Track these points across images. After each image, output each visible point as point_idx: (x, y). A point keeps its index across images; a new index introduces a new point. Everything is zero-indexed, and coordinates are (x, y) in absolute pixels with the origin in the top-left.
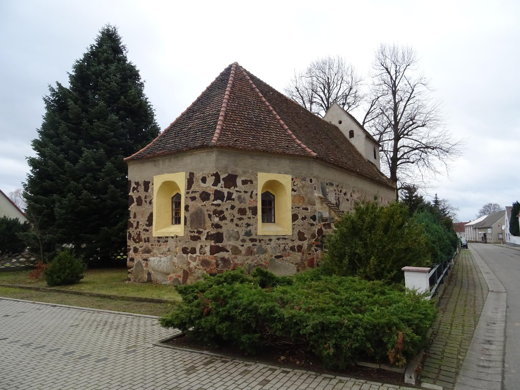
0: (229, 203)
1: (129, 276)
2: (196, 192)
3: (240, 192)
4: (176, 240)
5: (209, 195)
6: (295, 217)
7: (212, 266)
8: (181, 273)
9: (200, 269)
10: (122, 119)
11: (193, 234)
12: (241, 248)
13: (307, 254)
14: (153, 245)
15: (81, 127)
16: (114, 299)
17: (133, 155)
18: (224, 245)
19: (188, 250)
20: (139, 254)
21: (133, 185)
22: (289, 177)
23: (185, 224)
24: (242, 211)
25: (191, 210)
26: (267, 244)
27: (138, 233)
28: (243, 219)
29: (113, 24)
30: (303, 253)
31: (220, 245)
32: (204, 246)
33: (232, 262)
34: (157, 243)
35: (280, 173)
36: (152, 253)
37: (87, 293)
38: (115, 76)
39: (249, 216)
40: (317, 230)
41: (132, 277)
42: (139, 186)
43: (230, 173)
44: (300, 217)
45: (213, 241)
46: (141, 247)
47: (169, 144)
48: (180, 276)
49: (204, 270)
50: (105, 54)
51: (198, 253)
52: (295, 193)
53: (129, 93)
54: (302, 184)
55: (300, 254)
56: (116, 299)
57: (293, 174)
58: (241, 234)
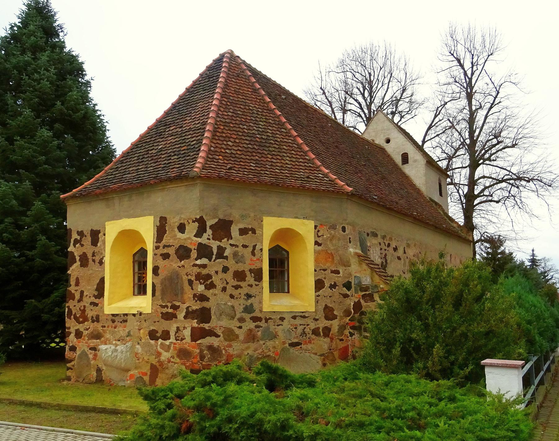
0: (220, 263)
1: (69, 373)
2: (169, 246)
4: (139, 319)
6: (319, 285)
7: (194, 358)
8: (146, 369)
9: (175, 363)
11: (165, 310)
12: (237, 331)
13: (338, 341)
14: (105, 327)
16: (46, 408)
17: (74, 190)
18: (212, 326)
19: (158, 335)
20: (84, 339)
21: (75, 236)
22: (311, 224)
23: (154, 294)
24: (240, 276)
25: (163, 273)
26: (278, 325)
27: (82, 308)
28: (241, 287)
30: (332, 339)
31: (206, 326)
32: (181, 329)
33: (224, 352)
34: (110, 323)
36: (103, 339)
39: (250, 283)
40: (352, 304)
42: (84, 238)
43: (221, 217)
44: (327, 285)
46: (87, 329)
50: (32, 38)
51: (172, 339)
52: (320, 248)
53: (69, 96)
54: (331, 234)
55: (327, 340)
56: (48, 409)
57: (316, 220)
58: (239, 310)
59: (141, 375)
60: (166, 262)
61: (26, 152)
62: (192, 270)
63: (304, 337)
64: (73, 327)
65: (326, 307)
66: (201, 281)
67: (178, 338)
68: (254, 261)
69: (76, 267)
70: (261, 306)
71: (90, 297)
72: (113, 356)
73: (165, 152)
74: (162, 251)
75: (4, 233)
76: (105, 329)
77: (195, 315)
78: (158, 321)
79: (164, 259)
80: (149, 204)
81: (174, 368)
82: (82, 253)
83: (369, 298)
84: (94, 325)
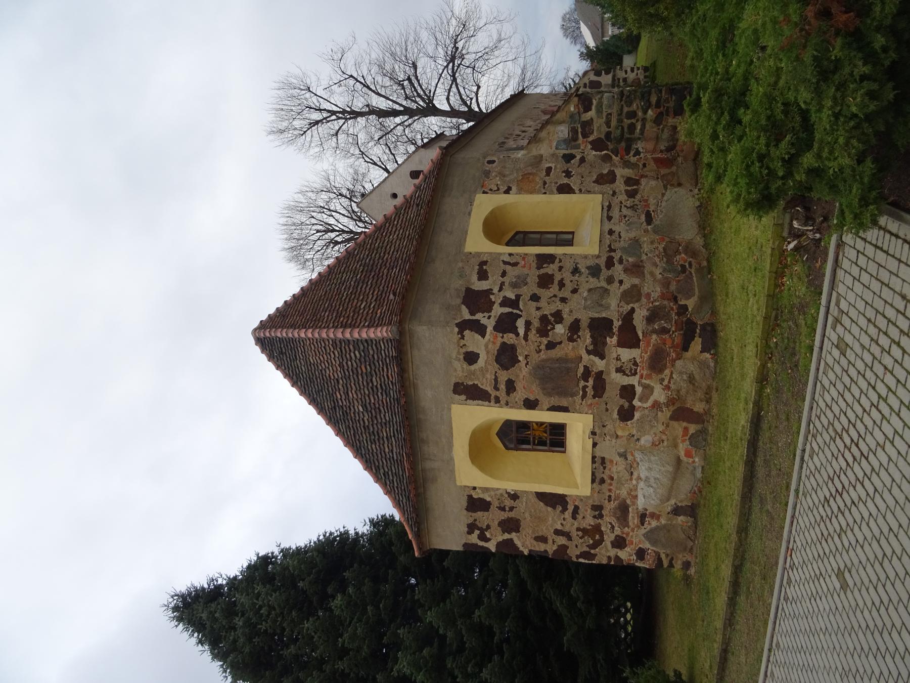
0: (525, 304)
1: (678, 565)
2: (496, 380)
3: (502, 284)
4: (600, 436)
5: (504, 344)
6: (565, 189)
7: (665, 344)
8: (678, 427)
9: (671, 377)
10: (343, 588)
11: (590, 392)
12: (626, 286)
13: (645, 169)
14: (610, 497)
15: (352, 675)
16: (742, 557)
17: (410, 537)
18: (617, 316)
19: (626, 405)
20: (628, 534)
21: (474, 539)
22: (480, 198)
23: (565, 410)
24: (545, 281)
25: (535, 392)
26: (620, 237)
27: (580, 533)
28: (562, 279)
29: (165, 599)
30: (642, 176)
31: (617, 324)
32: (619, 364)
33: (657, 304)
34: (605, 487)
35: (470, 214)
36: (628, 502)
37: (724, 635)
38: (259, 594)
39: (557, 269)
40: (594, 153)
41: (681, 556)
42: (477, 523)
43: (459, 301)
44: (566, 181)
45: (608, 339)
46: (613, 527)
47: (392, 451)
48: (686, 429)
49: (673, 366)
50: (217, 615)
51: (634, 380)
52: (514, 189)
53: (294, 571)
54: (496, 176)
55: (643, 181)
56: (744, 552)
57: (475, 192)
58: (593, 282)
59: (687, 438)
60: (519, 386)
61: (359, 631)
62: (532, 342)
63: (639, 207)
64: (608, 551)
65: (597, 182)
66: (549, 328)
67: (633, 372)
68: (525, 264)
69: (520, 540)
70: (590, 257)
71: (564, 519)
72: (654, 485)
73: (367, 398)
74: (502, 394)
75: (467, 670)
76: (613, 495)
77: (599, 339)
78: (606, 404)
79: (515, 390)
80: (434, 410)
81: (678, 379)
82: (499, 529)
83: (587, 126)
84: (606, 515)
